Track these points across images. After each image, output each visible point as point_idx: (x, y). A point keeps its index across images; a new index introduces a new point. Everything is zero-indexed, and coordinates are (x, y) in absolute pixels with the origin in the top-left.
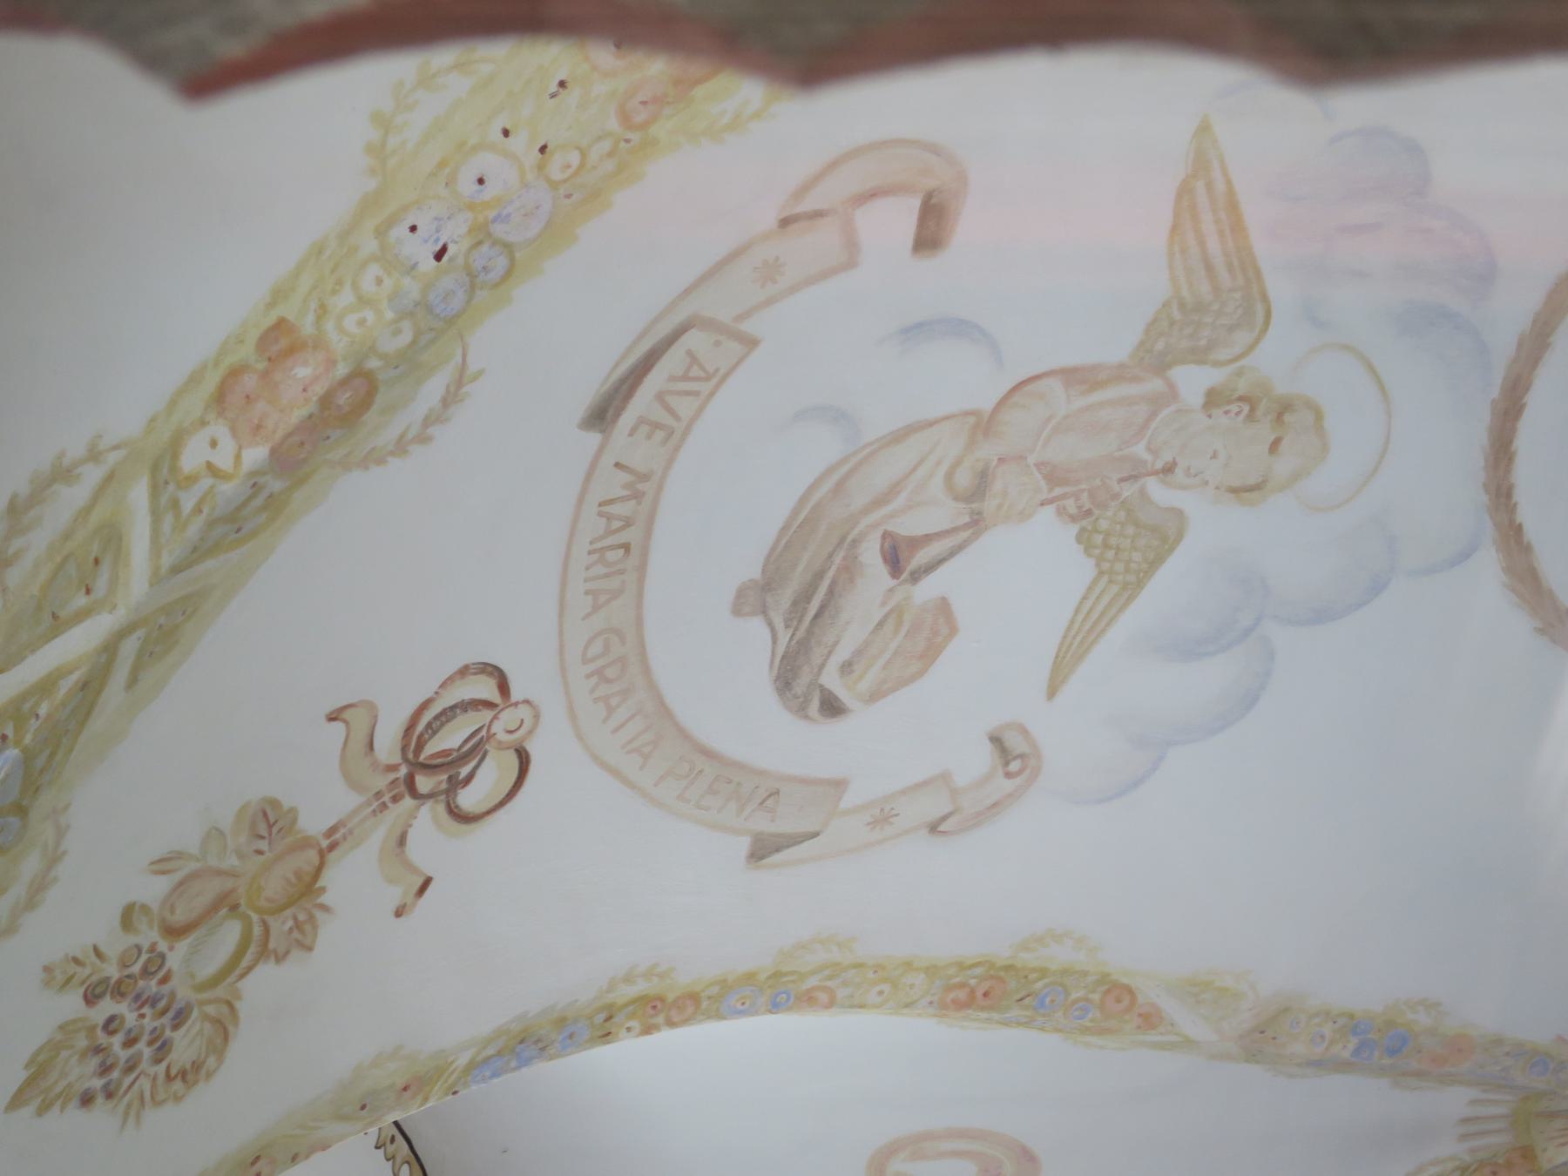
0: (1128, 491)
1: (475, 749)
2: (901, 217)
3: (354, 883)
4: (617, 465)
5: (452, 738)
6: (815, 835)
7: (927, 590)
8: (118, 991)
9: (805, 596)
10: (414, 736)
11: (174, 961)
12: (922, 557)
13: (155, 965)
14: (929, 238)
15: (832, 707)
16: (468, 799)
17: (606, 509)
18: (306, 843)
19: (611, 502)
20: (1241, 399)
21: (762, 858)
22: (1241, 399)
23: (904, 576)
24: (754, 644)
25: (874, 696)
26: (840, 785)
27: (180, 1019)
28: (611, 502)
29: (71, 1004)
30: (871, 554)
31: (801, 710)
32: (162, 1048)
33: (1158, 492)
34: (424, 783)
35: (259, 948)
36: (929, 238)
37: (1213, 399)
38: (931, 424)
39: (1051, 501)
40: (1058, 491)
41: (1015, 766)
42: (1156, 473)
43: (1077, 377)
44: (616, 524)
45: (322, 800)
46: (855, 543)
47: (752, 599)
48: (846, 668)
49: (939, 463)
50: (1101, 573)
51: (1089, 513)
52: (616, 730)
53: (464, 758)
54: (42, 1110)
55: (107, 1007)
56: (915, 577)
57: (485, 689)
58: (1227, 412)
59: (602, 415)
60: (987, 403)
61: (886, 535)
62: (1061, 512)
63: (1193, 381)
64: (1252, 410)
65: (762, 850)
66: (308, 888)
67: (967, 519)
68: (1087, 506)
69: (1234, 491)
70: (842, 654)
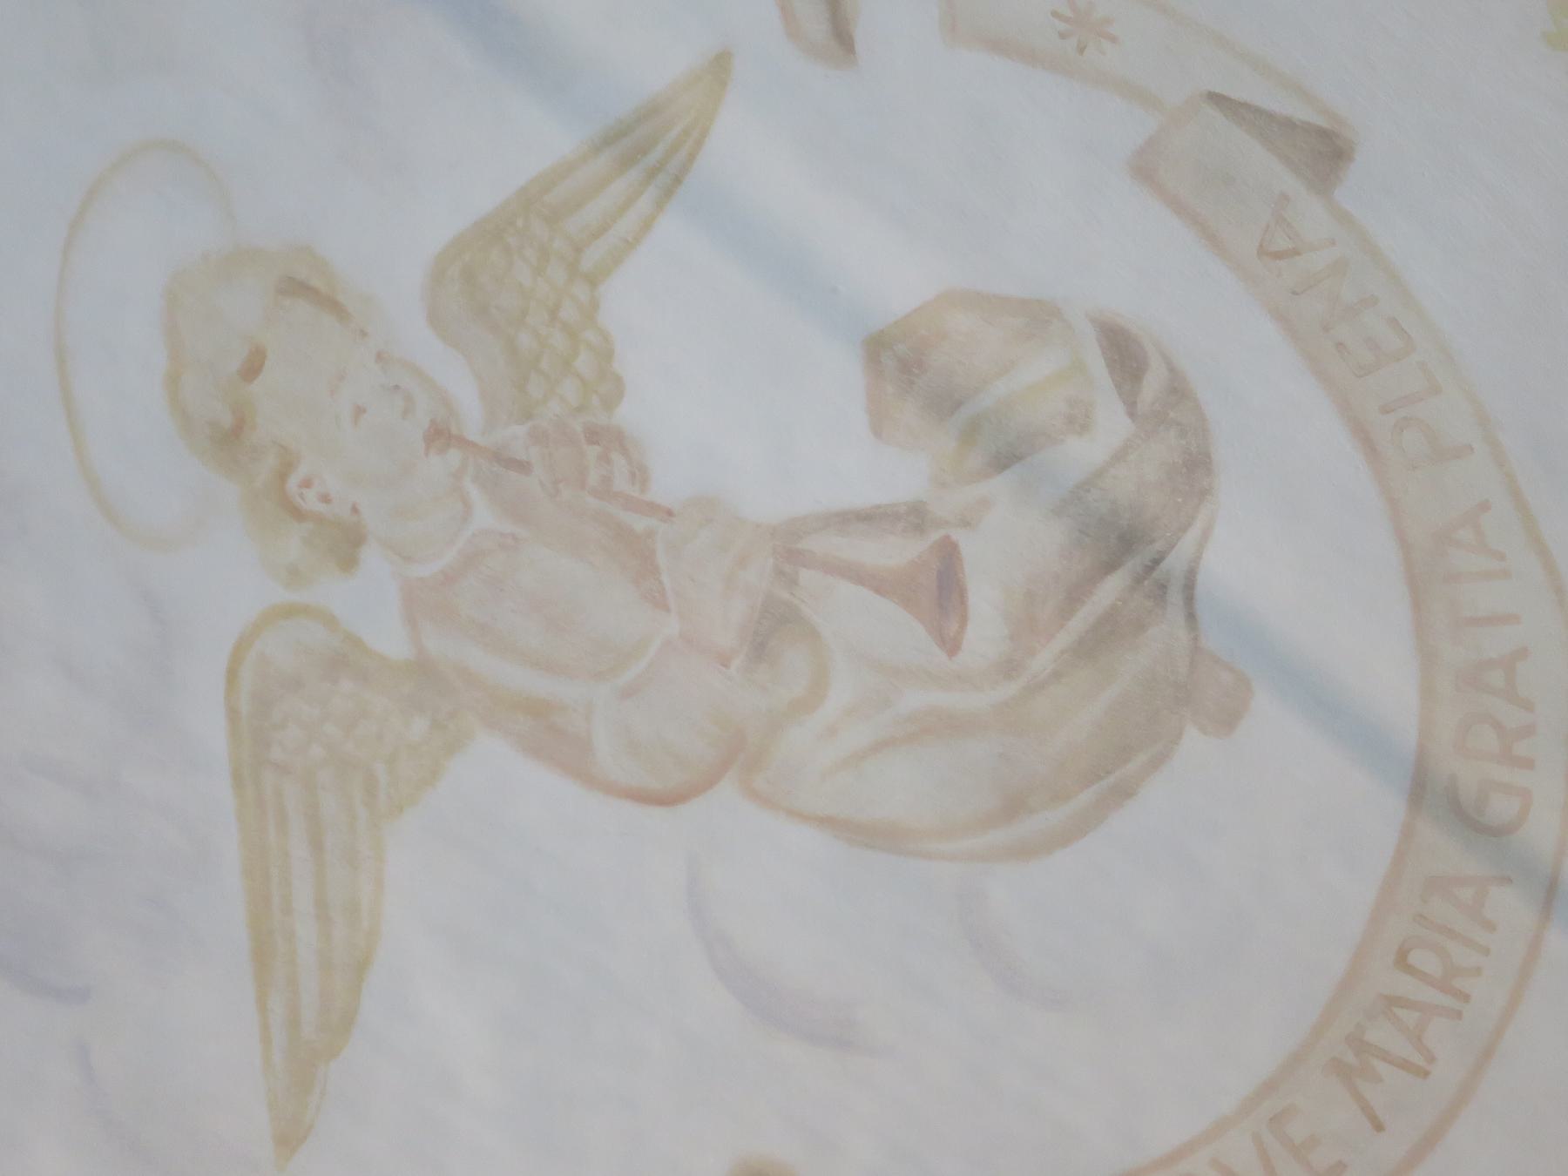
0: (515, 435)
4: (1379, 1127)
6: (1216, 99)
12: (893, 552)
17: (1418, 1060)
19: (1405, 1065)
20: (298, 514)
21: (1324, 134)
22: (298, 514)
23: (935, 536)
28: (1405, 1065)
30: (985, 629)
33: (462, 387)
37: (344, 544)
38: (827, 822)
39: (652, 508)
40: (640, 524)
42: (462, 442)
43: (552, 738)
44: (1409, 1017)
46: (1009, 668)
50: (593, 281)
51: (593, 435)
52: (1486, 951)
56: (914, 518)
58: (325, 499)
61: (947, 537)
62: (640, 475)
63: (369, 604)
64: (282, 476)
67: (806, 576)
68: (593, 451)
69: (331, 304)
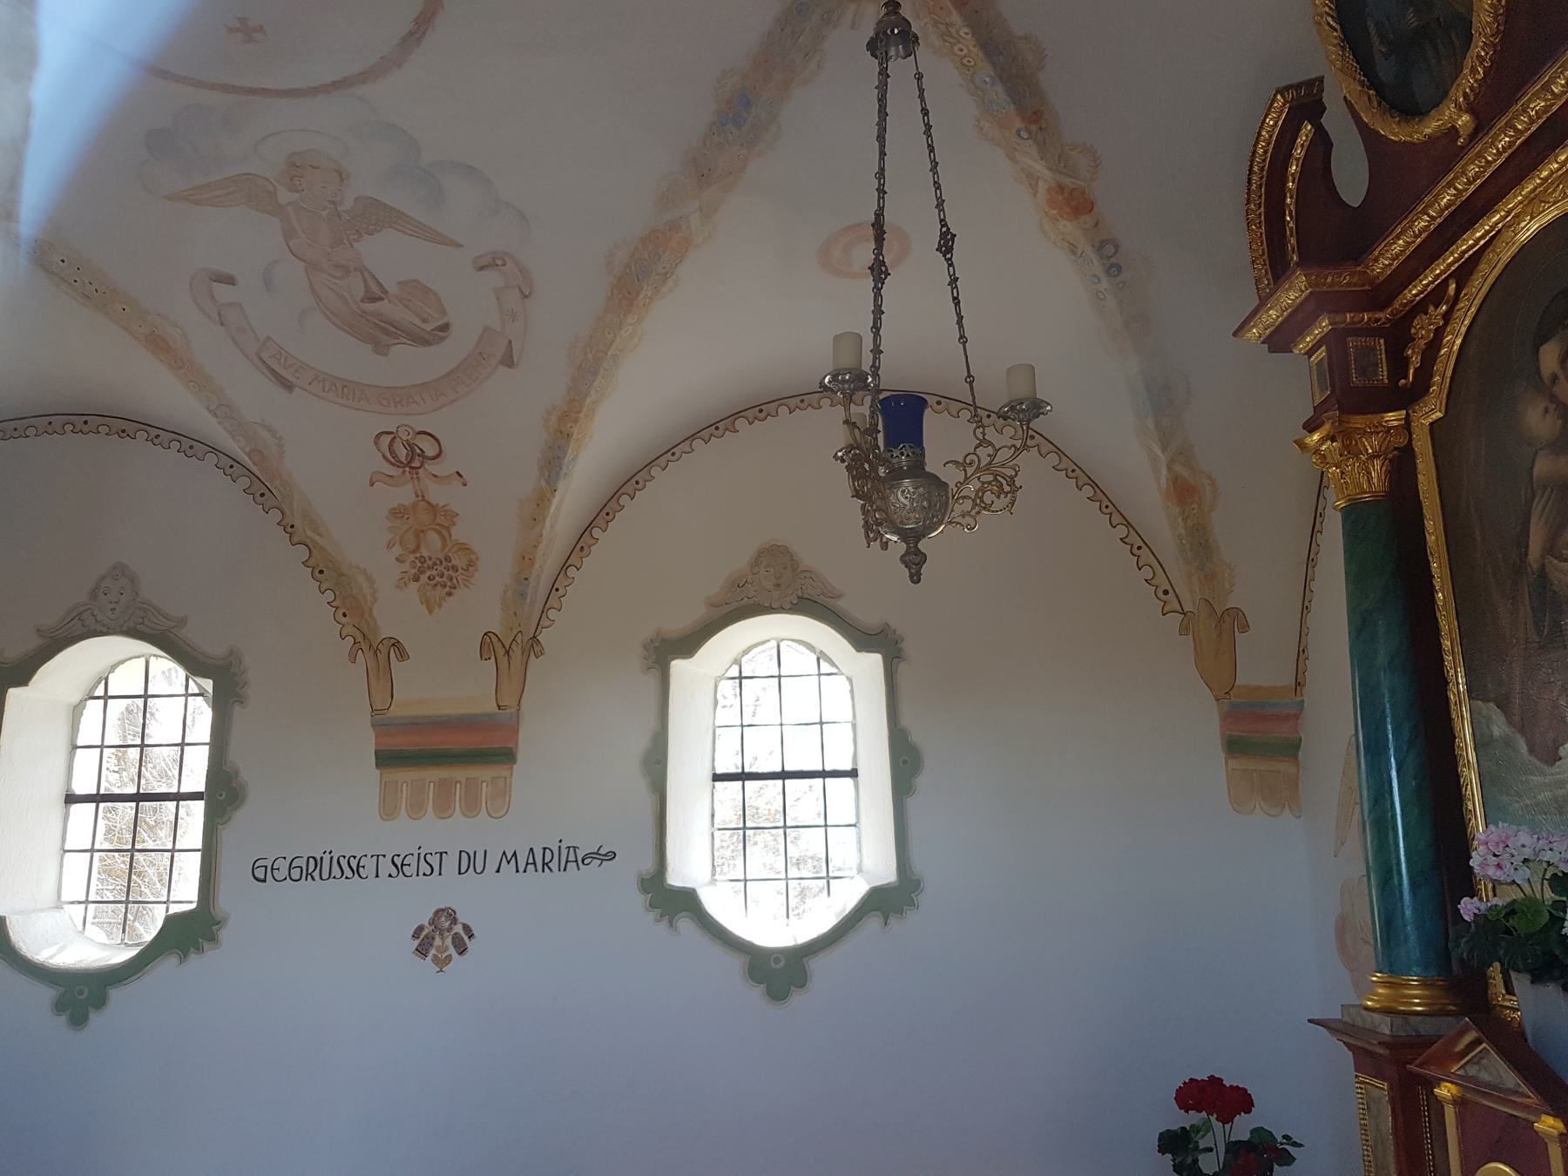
1: (411, 447)
2: (221, 290)
3: (437, 494)
5: (402, 453)
7: (392, 289)
8: (422, 572)
9: (387, 333)
10: (397, 463)
11: (425, 553)
13: (422, 560)
14: (230, 281)
15: (445, 328)
16: (430, 452)
18: (415, 505)
24: (403, 352)
25: (443, 312)
26: (486, 329)
27: (448, 559)
29: (414, 586)
31: (442, 339)
32: (455, 568)
34: (416, 464)
35: (444, 532)
36: (230, 281)
37: (293, 189)
41: (499, 262)
45: (404, 495)
47: (380, 349)
48: (424, 321)
49: (1464, 273)
53: (413, 450)
54: (440, 606)
55: (424, 578)
56: (386, 292)
57: (386, 440)
59: (289, 387)
60: (870, 258)
63: (284, 196)
65: (509, 361)
66: (433, 509)
70: (418, 322)
